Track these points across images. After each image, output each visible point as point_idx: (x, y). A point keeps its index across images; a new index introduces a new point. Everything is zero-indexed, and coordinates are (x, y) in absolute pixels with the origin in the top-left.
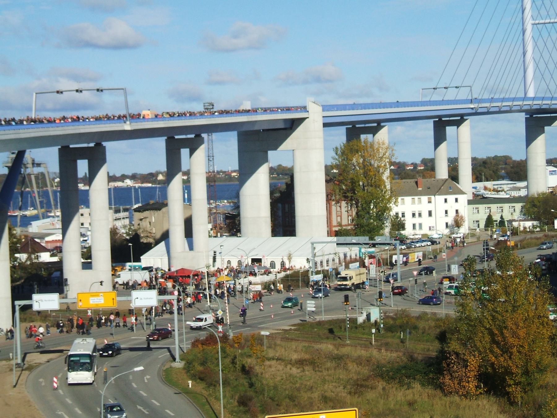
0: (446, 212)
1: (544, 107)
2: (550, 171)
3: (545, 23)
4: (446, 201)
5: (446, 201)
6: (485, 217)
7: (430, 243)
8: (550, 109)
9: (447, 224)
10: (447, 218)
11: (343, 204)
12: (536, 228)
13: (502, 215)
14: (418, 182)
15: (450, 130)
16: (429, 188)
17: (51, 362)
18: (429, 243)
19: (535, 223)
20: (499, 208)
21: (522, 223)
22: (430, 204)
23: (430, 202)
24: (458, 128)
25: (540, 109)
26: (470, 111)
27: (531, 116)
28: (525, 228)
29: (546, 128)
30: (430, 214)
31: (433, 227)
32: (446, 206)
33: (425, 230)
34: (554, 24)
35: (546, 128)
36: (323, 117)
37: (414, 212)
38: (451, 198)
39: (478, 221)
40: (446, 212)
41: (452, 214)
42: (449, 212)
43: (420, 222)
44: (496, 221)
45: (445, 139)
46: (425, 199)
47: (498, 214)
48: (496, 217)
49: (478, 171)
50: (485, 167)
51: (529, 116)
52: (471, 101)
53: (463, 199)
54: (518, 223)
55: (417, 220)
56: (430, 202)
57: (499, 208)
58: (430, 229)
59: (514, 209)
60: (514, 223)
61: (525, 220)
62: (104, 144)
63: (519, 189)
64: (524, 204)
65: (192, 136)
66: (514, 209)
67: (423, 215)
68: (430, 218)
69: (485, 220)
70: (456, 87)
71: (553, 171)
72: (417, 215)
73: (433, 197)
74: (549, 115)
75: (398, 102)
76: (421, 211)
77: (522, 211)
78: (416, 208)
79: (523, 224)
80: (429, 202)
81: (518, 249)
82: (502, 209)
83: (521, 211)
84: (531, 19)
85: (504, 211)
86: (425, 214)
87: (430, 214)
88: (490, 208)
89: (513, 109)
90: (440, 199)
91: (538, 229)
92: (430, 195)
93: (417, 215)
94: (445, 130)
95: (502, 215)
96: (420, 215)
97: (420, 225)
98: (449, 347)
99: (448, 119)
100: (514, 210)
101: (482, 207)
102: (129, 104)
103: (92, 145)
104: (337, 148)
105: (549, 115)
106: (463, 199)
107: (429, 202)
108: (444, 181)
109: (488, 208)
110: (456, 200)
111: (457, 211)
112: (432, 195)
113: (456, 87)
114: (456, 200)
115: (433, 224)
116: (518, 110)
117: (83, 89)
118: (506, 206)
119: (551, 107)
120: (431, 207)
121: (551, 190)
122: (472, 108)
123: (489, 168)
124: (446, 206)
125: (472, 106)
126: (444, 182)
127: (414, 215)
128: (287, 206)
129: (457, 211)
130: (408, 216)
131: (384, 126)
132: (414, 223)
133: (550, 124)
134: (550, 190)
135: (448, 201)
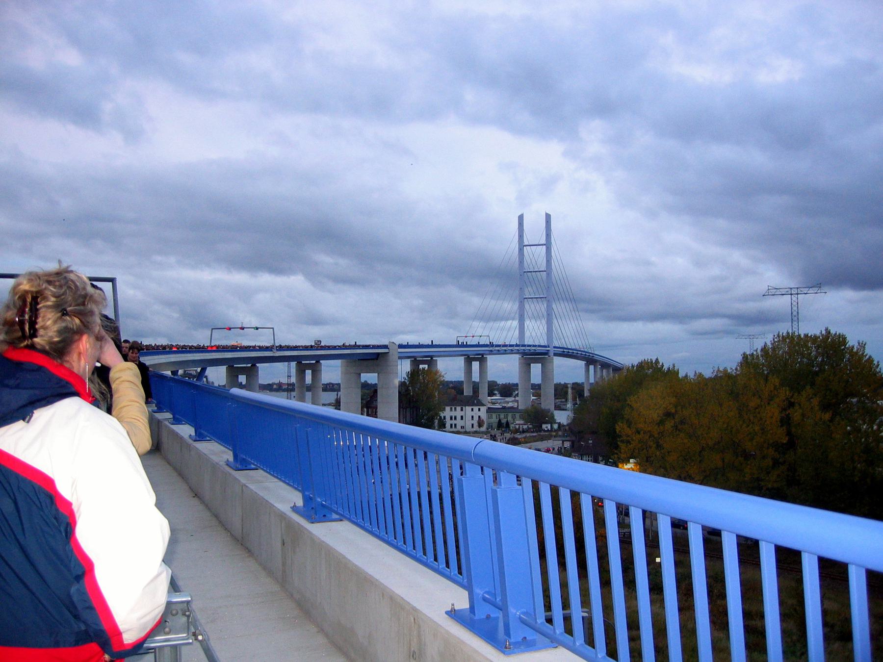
0: (472, 417)
3: (532, 298)
11: (408, 410)
17: (381, 484)
28: (523, 429)
30: (462, 417)
32: (472, 413)
38: (476, 408)
40: (472, 417)
41: (476, 418)
42: (474, 417)
46: (459, 408)
48: (504, 421)
53: (484, 409)
55: (453, 422)
58: (461, 428)
62: (258, 365)
63: (508, 402)
65: (314, 362)
78: (453, 414)
86: (459, 418)
90: (468, 408)
96: (455, 418)
97: (455, 425)
98: (875, 364)
101: (494, 415)
102: (120, 303)
103: (249, 365)
104: (409, 372)
106: (484, 409)
111: (479, 417)
115: (463, 424)
117: (245, 327)
120: (462, 413)
124: (472, 413)
127: (451, 418)
128: (370, 410)
130: (448, 418)
132: (451, 423)
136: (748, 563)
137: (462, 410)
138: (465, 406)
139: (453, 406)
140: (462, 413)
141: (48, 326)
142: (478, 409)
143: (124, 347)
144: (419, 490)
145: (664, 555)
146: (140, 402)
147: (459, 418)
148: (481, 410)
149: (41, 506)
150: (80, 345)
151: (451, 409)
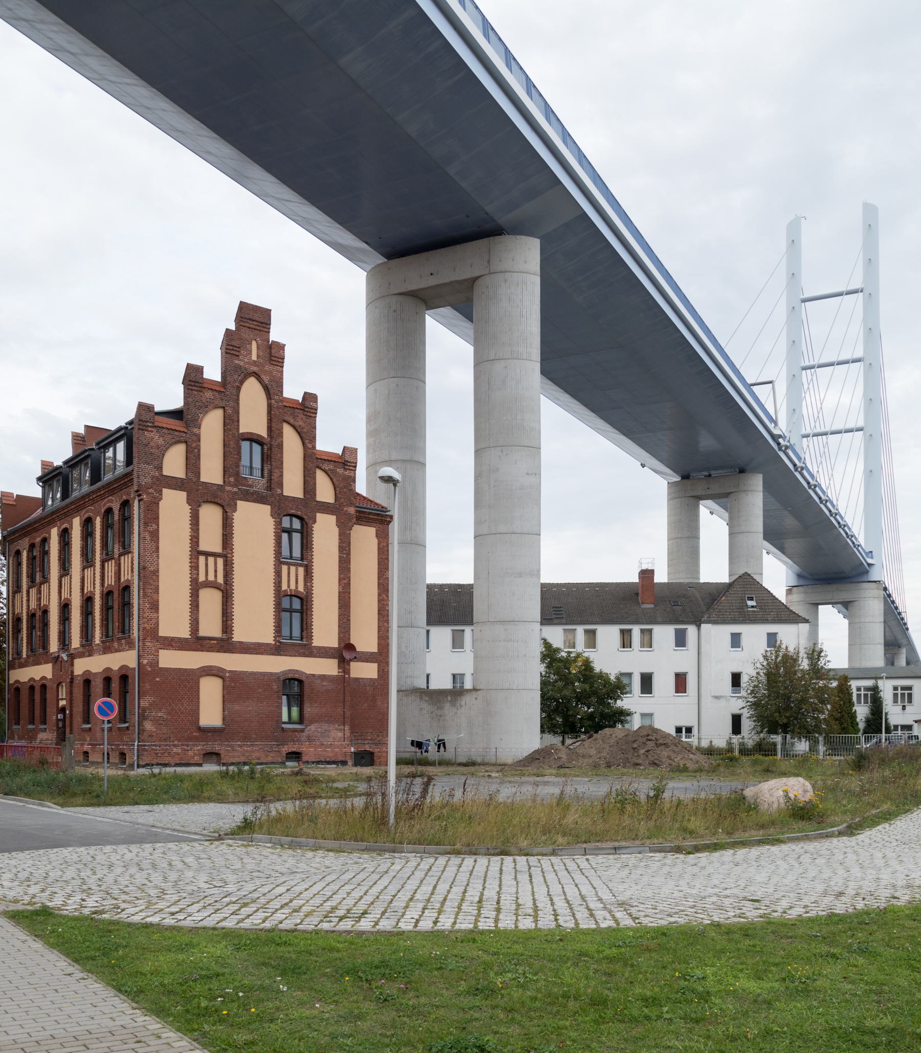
30: (681, 682)
46: (664, 633)
86: (664, 683)
120: (684, 660)
136: (562, 845)
137: (681, 640)
138: (698, 623)
139: (637, 622)
140: (684, 660)
141: (441, 708)
142: (728, 639)
143: (729, 743)
144: (305, 758)
145: (429, 795)
146: (183, 922)
147: (664, 683)
148: (744, 641)
149: (99, 74)
150: (104, 920)
151: (626, 637)
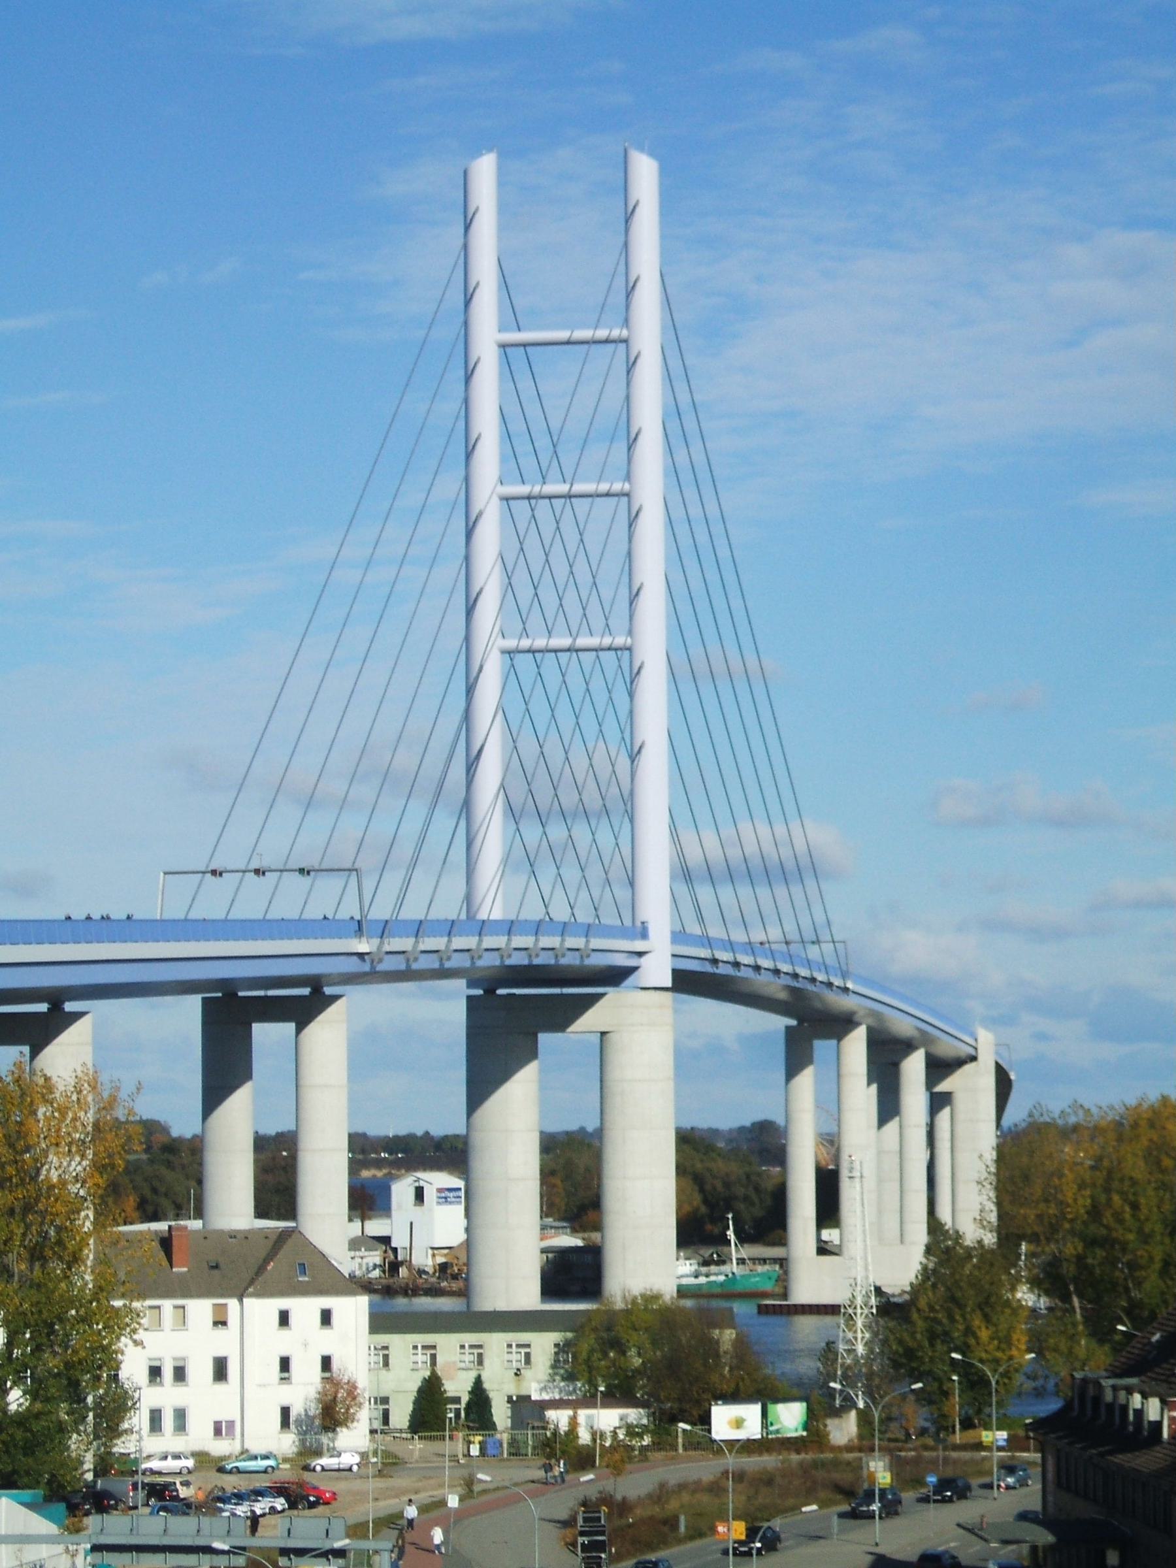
0: (285, 1364)
1: (569, 960)
2: (440, 1190)
4: (284, 1319)
5: (284, 1319)
6: (413, 1384)
7: (282, 1500)
8: (557, 968)
9: (285, 1412)
10: (285, 1387)
12: (640, 1436)
13: (478, 1382)
14: (175, 1242)
15: (822, 1047)
16: (216, 1267)
18: (280, 1503)
19: (634, 1415)
20: (467, 1350)
21: (583, 1414)
22: (220, 1332)
23: (221, 1323)
24: (299, 1031)
25: (531, 967)
26: (353, 965)
27: (490, 992)
29: (544, 1038)
30: (220, 1370)
31: (231, 1424)
32: (285, 1341)
33: (200, 1437)
34: (601, 654)
35: (544, 1038)
36: (673, 956)
37: (180, 1364)
39: (385, 1400)
40: (285, 1364)
42: (294, 1365)
43: (180, 1404)
44: (457, 1400)
45: (247, 1075)
46: (201, 1309)
47: (462, 1375)
49: (146, 1180)
50: (169, 1165)
51: (481, 992)
52: (359, 928)
54: (570, 1412)
56: (221, 1323)
57: (467, 1350)
58: (218, 1431)
59: (528, 1355)
60: (551, 1414)
61: (589, 1401)
64: (569, 1335)
66: (528, 1355)
67: (190, 1372)
68: (220, 1387)
69: (412, 1397)
70: (301, 871)
71: (450, 1190)
72: (168, 1373)
73: (233, 1304)
74: (557, 991)
75: (68, 918)
76: (184, 1359)
77: (557, 1361)
79: (589, 1417)
80: (216, 1323)
81: (680, 1541)
82: (480, 1356)
83: (555, 1366)
84: (500, 635)
85: (486, 1362)
86: (198, 1371)
87: (220, 1370)
88: (434, 1347)
89: (380, 967)
91: (647, 1440)
92: (222, 1296)
93: (168, 1373)
94: (811, 1048)
95: (478, 1382)
96: (180, 1374)
97: (181, 1415)
99: (261, 993)
100: (528, 1358)
105: (557, 991)
107: (216, 1323)
108: (274, 1237)
109: (424, 1347)
110: (326, 1318)
112: (230, 1296)
113: (301, 871)
114: (326, 1318)
116: (434, 970)
118: (496, 1342)
119: (587, 962)
120: (224, 1343)
121: (443, 1260)
122: (361, 956)
123: (183, 1167)
124: (285, 1341)
125: (363, 947)
126: (270, 1243)
129: (326, 1363)
131: (77, 1016)
133: (561, 1025)
134: (440, 1260)
135: (293, 1319)
